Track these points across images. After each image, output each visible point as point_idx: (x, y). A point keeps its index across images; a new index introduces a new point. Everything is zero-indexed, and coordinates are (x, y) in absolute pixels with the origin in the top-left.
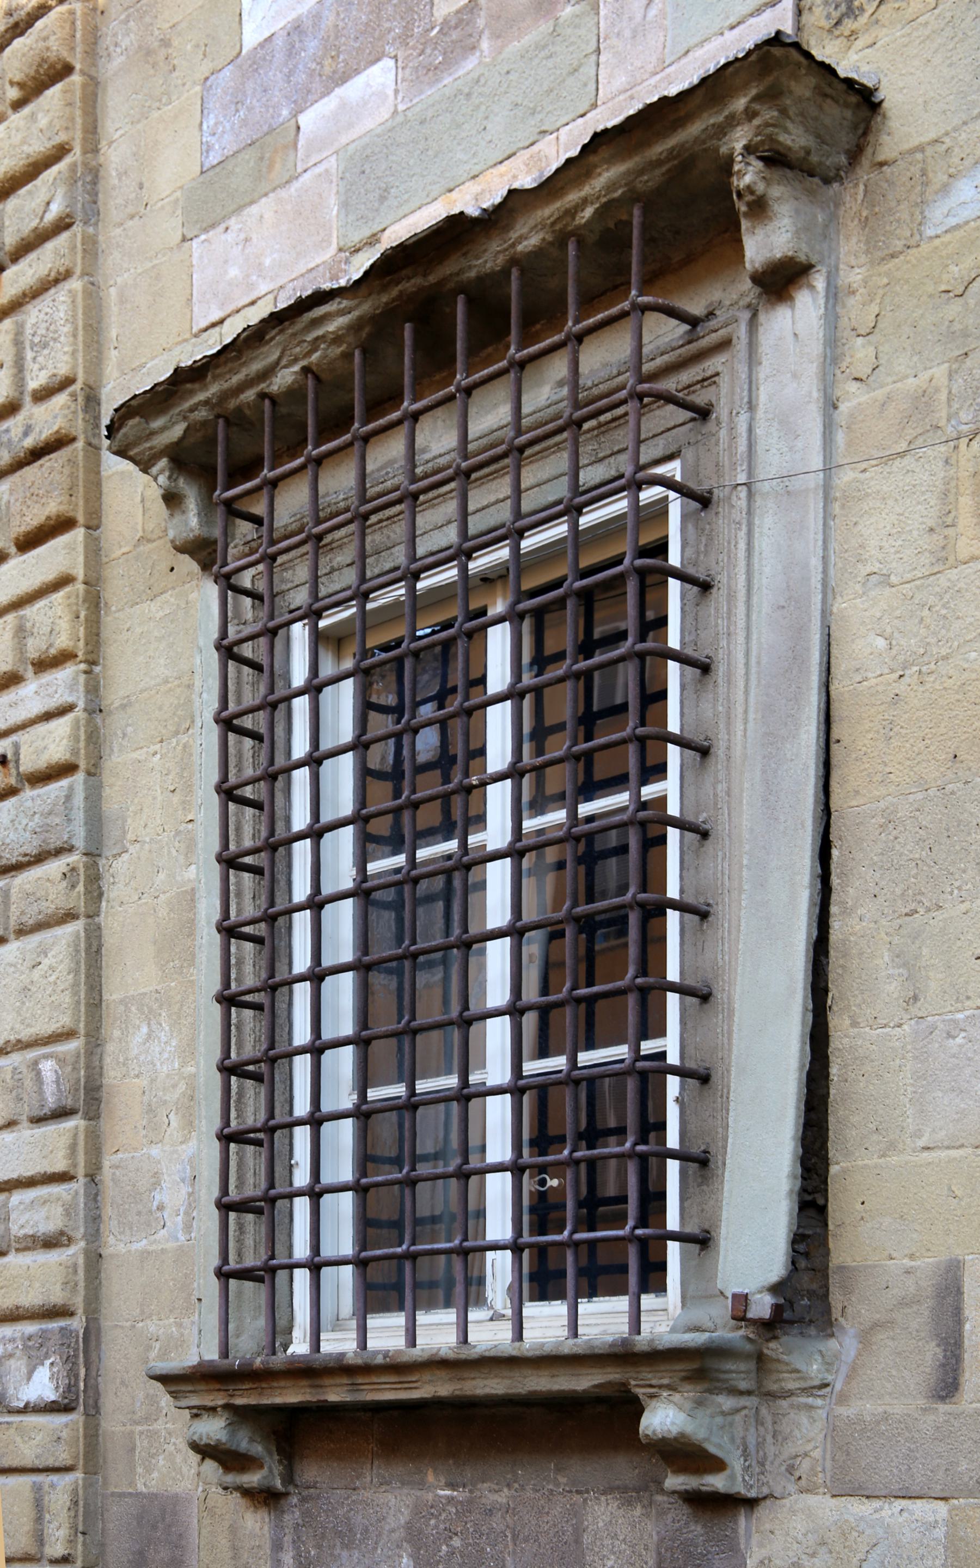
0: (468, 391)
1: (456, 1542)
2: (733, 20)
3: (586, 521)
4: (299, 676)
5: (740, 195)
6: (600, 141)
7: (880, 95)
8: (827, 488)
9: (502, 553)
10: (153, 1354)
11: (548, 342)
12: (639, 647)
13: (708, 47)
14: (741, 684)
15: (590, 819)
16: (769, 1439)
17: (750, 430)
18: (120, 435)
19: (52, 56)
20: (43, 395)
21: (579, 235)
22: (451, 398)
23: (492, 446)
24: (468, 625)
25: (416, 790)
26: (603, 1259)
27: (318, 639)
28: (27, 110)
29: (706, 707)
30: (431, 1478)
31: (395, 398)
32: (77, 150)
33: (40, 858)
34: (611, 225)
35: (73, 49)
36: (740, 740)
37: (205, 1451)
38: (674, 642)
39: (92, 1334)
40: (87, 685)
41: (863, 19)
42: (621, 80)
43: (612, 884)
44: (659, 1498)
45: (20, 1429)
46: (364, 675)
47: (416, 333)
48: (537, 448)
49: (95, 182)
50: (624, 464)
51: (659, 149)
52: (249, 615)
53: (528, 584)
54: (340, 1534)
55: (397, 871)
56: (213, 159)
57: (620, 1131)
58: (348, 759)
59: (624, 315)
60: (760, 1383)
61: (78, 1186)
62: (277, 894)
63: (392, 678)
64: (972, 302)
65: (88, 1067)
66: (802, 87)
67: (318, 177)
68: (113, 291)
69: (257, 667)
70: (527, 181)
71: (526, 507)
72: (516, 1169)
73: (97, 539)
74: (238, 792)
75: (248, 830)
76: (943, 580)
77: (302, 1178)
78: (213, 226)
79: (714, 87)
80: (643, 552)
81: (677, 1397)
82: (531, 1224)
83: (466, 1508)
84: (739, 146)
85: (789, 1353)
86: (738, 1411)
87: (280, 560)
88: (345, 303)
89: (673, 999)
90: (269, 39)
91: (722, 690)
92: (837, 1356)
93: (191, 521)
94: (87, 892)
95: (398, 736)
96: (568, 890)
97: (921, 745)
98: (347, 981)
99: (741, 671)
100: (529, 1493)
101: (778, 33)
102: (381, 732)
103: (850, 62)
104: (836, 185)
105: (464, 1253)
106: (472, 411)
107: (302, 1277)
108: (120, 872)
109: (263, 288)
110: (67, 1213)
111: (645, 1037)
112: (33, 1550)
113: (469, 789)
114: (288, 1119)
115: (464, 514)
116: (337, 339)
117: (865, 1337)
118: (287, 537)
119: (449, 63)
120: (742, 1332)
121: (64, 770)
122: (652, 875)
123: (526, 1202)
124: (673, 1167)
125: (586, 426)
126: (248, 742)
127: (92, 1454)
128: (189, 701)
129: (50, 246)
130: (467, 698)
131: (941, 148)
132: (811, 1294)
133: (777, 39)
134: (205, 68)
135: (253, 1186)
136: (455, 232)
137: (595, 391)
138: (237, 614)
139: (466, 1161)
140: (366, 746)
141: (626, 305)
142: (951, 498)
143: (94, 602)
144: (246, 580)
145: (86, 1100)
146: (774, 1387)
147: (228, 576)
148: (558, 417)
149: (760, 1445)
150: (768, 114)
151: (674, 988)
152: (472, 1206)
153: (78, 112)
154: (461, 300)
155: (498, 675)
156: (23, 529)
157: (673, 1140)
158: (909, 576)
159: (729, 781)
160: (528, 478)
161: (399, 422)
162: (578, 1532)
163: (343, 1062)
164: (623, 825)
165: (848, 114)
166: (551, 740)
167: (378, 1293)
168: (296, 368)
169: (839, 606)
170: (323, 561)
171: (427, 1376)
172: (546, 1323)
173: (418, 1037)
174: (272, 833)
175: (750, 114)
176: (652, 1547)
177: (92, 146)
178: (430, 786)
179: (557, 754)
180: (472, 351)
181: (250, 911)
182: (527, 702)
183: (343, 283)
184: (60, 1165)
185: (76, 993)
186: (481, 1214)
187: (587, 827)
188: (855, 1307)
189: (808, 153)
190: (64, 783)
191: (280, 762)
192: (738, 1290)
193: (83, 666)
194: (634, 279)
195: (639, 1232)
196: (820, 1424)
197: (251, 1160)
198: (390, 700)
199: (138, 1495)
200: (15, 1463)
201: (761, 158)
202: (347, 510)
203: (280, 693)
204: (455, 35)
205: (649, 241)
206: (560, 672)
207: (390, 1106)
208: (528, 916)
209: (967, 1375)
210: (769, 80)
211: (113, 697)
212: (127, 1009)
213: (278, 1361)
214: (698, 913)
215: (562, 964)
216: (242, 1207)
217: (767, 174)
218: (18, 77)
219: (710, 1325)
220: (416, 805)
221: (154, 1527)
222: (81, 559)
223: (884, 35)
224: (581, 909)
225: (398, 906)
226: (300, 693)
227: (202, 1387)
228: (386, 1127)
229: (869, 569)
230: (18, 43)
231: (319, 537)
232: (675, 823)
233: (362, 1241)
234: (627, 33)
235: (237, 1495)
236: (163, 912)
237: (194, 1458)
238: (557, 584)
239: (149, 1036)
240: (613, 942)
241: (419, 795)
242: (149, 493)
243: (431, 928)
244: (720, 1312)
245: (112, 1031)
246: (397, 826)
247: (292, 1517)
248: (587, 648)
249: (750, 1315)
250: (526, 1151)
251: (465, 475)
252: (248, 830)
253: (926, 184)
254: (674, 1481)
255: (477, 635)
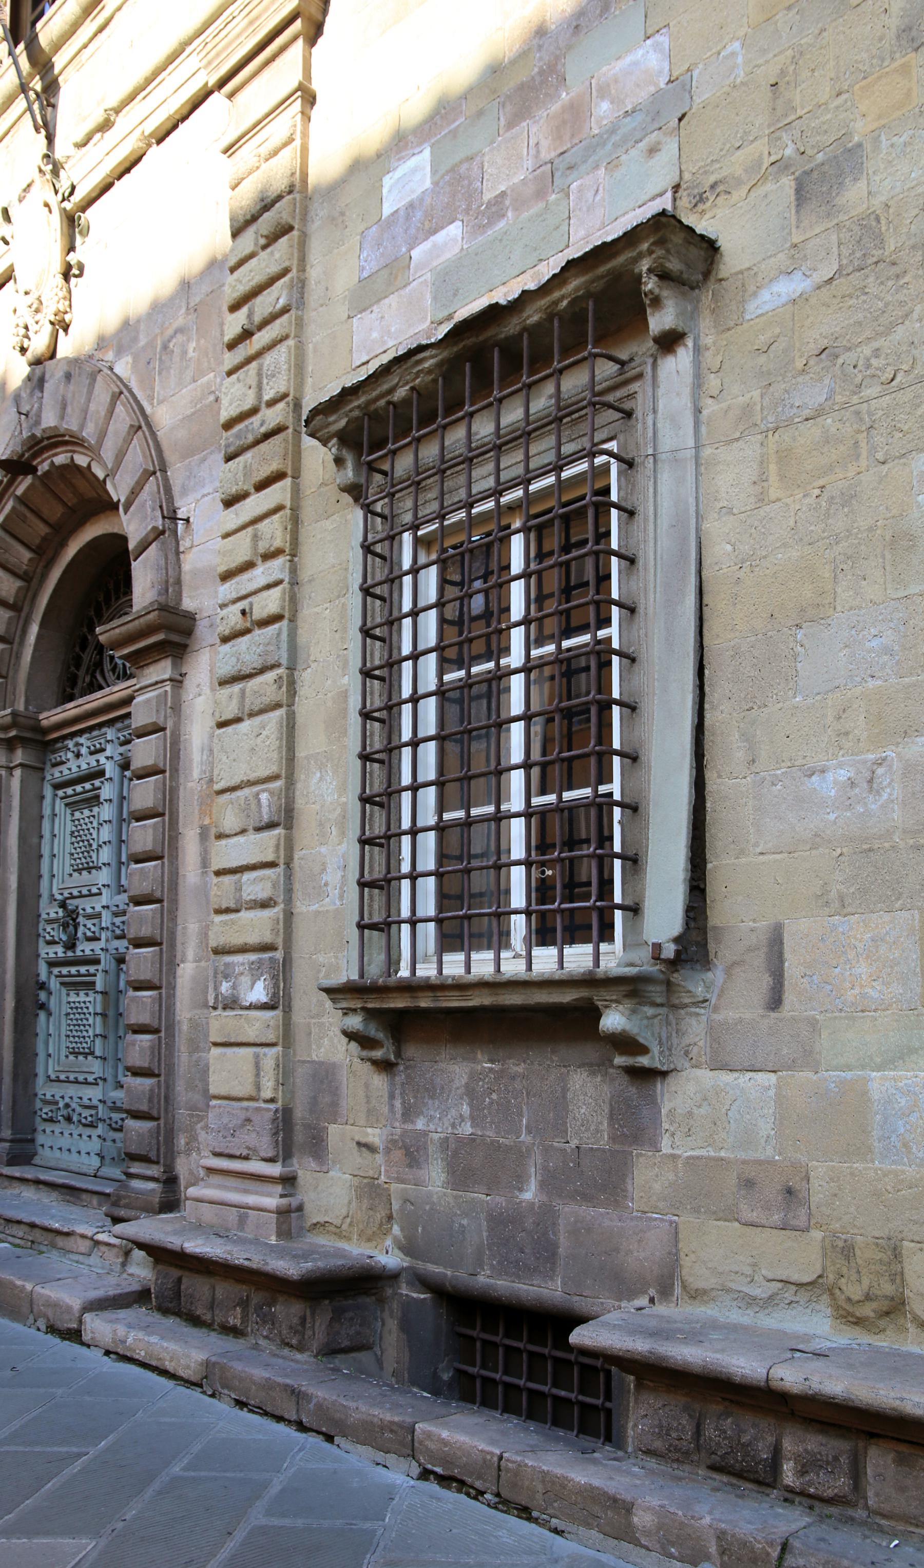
0: (500, 401)
1: (494, 1096)
2: (640, 203)
3: (565, 475)
4: (407, 564)
5: (646, 295)
6: (571, 265)
7: (719, 244)
8: (697, 458)
9: (519, 493)
10: (321, 975)
11: (543, 373)
12: (596, 548)
13: (627, 216)
14: (652, 571)
15: (569, 650)
16: (674, 1034)
17: (654, 424)
18: (312, 425)
19: (283, 222)
20: (271, 403)
21: (560, 315)
22: (491, 404)
23: (513, 432)
24: (500, 534)
25: (471, 633)
26: (578, 920)
27: (417, 541)
28: (269, 250)
29: (633, 584)
30: (479, 1056)
31: (461, 405)
32: (294, 270)
33: (262, 671)
34: (577, 309)
35: (294, 218)
36: (652, 603)
37: (351, 1036)
38: (614, 545)
39: (287, 962)
40: (290, 568)
41: (709, 204)
42: (582, 233)
43: (584, 689)
44: (611, 1070)
45: (247, 1019)
46: (443, 563)
47: (472, 368)
48: (538, 433)
49: (303, 287)
50: (585, 443)
51: (602, 269)
52: (379, 528)
53: (534, 511)
54: (427, 1090)
55: (460, 680)
56: (365, 274)
57: (588, 841)
58: (433, 613)
59: (584, 359)
60: (668, 998)
61: (280, 870)
62: (393, 693)
63: (458, 564)
64: (772, 356)
65: (287, 797)
66: (678, 238)
67: (421, 284)
68: (310, 345)
69: (383, 558)
70: (532, 286)
71: (532, 466)
72: (528, 863)
73: (298, 484)
74: (372, 632)
75: (377, 655)
76: (762, 512)
77: (406, 868)
78: (364, 310)
79: (631, 237)
80: (597, 493)
81: (621, 1007)
82: (537, 899)
83: (500, 1075)
84: (645, 269)
85: (685, 980)
86: (656, 1016)
87: (397, 496)
88: (434, 352)
89: (616, 760)
90: (396, 212)
91: (641, 573)
92: (712, 983)
93: (349, 474)
94: (288, 691)
95: (461, 599)
96: (557, 692)
97: (753, 608)
98: (432, 746)
99: (652, 563)
100: (536, 1067)
101: (664, 210)
102: (451, 597)
103: (701, 228)
104: (697, 291)
105: (498, 915)
106: (502, 412)
107: (405, 929)
108: (306, 678)
109: (390, 344)
110: (274, 887)
111: (601, 783)
112: (254, 1094)
113: (501, 631)
114: (398, 831)
115: (498, 470)
116: (429, 371)
117: (728, 971)
118: (401, 483)
119: (491, 224)
120: (658, 967)
121: (275, 618)
122: (604, 684)
123: (533, 884)
124: (617, 863)
125: (565, 421)
126: (378, 602)
127: (287, 1037)
128: (346, 578)
129: (278, 322)
130: (499, 577)
131: (753, 272)
132: (697, 944)
133: (663, 213)
134: (362, 228)
135: (378, 873)
136: (493, 313)
137: (569, 401)
138: (373, 527)
139: (499, 859)
140: (443, 605)
141: (586, 354)
142: (765, 465)
143: (296, 520)
144: (378, 507)
145: (285, 818)
146: (677, 1002)
147: (368, 505)
148: (549, 415)
149: (669, 1038)
150: (660, 252)
151: (617, 753)
152: (502, 887)
153: (296, 251)
154: (496, 350)
155: (517, 564)
156: (259, 478)
157: (617, 848)
158: (743, 509)
159: (646, 628)
160: (533, 450)
161: (463, 418)
162: (565, 1090)
163: (429, 796)
164: (587, 654)
165: (702, 253)
166: (547, 602)
167: (450, 940)
168: (407, 388)
169: (706, 526)
170: (420, 497)
171: (477, 992)
172: (545, 960)
173: (472, 782)
174: (390, 656)
175: (650, 252)
176: (607, 1101)
177: (302, 268)
178: (479, 629)
179: (550, 611)
180: (502, 379)
181: (378, 704)
182: (533, 580)
183: (433, 340)
184: (270, 858)
185: (280, 752)
186: (508, 892)
187: (567, 654)
188: (724, 952)
189: (682, 273)
190: (277, 626)
191: (396, 614)
192: (655, 941)
193: (288, 558)
194: (590, 339)
195: (598, 904)
196: (703, 1025)
197: (377, 855)
198: (457, 578)
199: (313, 1062)
200: (244, 1040)
201: (656, 275)
202: (434, 467)
203: (396, 573)
204: (494, 209)
205: (597, 319)
206: (551, 562)
207: (456, 823)
208: (535, 708)
209: (786, 994)
210: (659, 234)
211: (304, 575)
212: (309, 763)
213: (392, 980)
214: (630, 707)
215: (553, 740)
216: (372, 885)
217: (660, 283)
218: (265, 233)
219: (639, 962)
220: (470, 641)
221: (322, 1082)
222: (289, 496)
223: (720, 213)
224: (564, 704)
225: (460, 701)
226: (407, 573)
227: (349, 996)
228: (454, 836)
229: (721, 505)
230: (266, 215)
231: (419, 483)
232: (616, 653)
233: (440, 907)
234: (585, 209)
235: (369, 1063)
236: (329, 704)
237: (345, 1040)
238: (549, 511)
239: (321, 779)
240: (583, 726)
241: (473, 634)
242: (326, 458)
243: (479, 714)
244: (645, 954)
245: (300, 776)
246: (460, 653)
247: (400, 1078)
248: (566, 548)
249: (662, 956)
250: (533, 853)
251: (499, 447)
252: (377, 655)
253: (744, 291)
254: (619, 1060)
255: (505, 541)
